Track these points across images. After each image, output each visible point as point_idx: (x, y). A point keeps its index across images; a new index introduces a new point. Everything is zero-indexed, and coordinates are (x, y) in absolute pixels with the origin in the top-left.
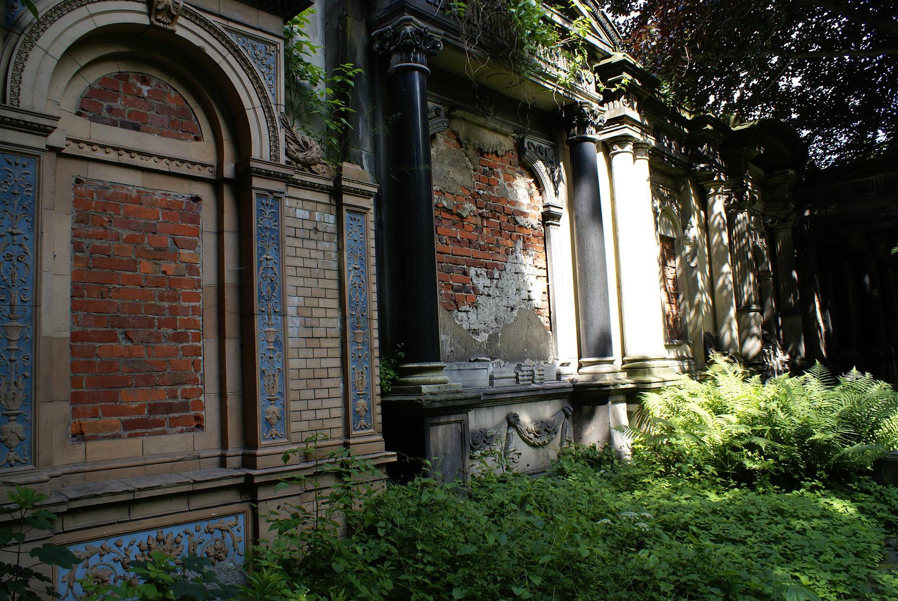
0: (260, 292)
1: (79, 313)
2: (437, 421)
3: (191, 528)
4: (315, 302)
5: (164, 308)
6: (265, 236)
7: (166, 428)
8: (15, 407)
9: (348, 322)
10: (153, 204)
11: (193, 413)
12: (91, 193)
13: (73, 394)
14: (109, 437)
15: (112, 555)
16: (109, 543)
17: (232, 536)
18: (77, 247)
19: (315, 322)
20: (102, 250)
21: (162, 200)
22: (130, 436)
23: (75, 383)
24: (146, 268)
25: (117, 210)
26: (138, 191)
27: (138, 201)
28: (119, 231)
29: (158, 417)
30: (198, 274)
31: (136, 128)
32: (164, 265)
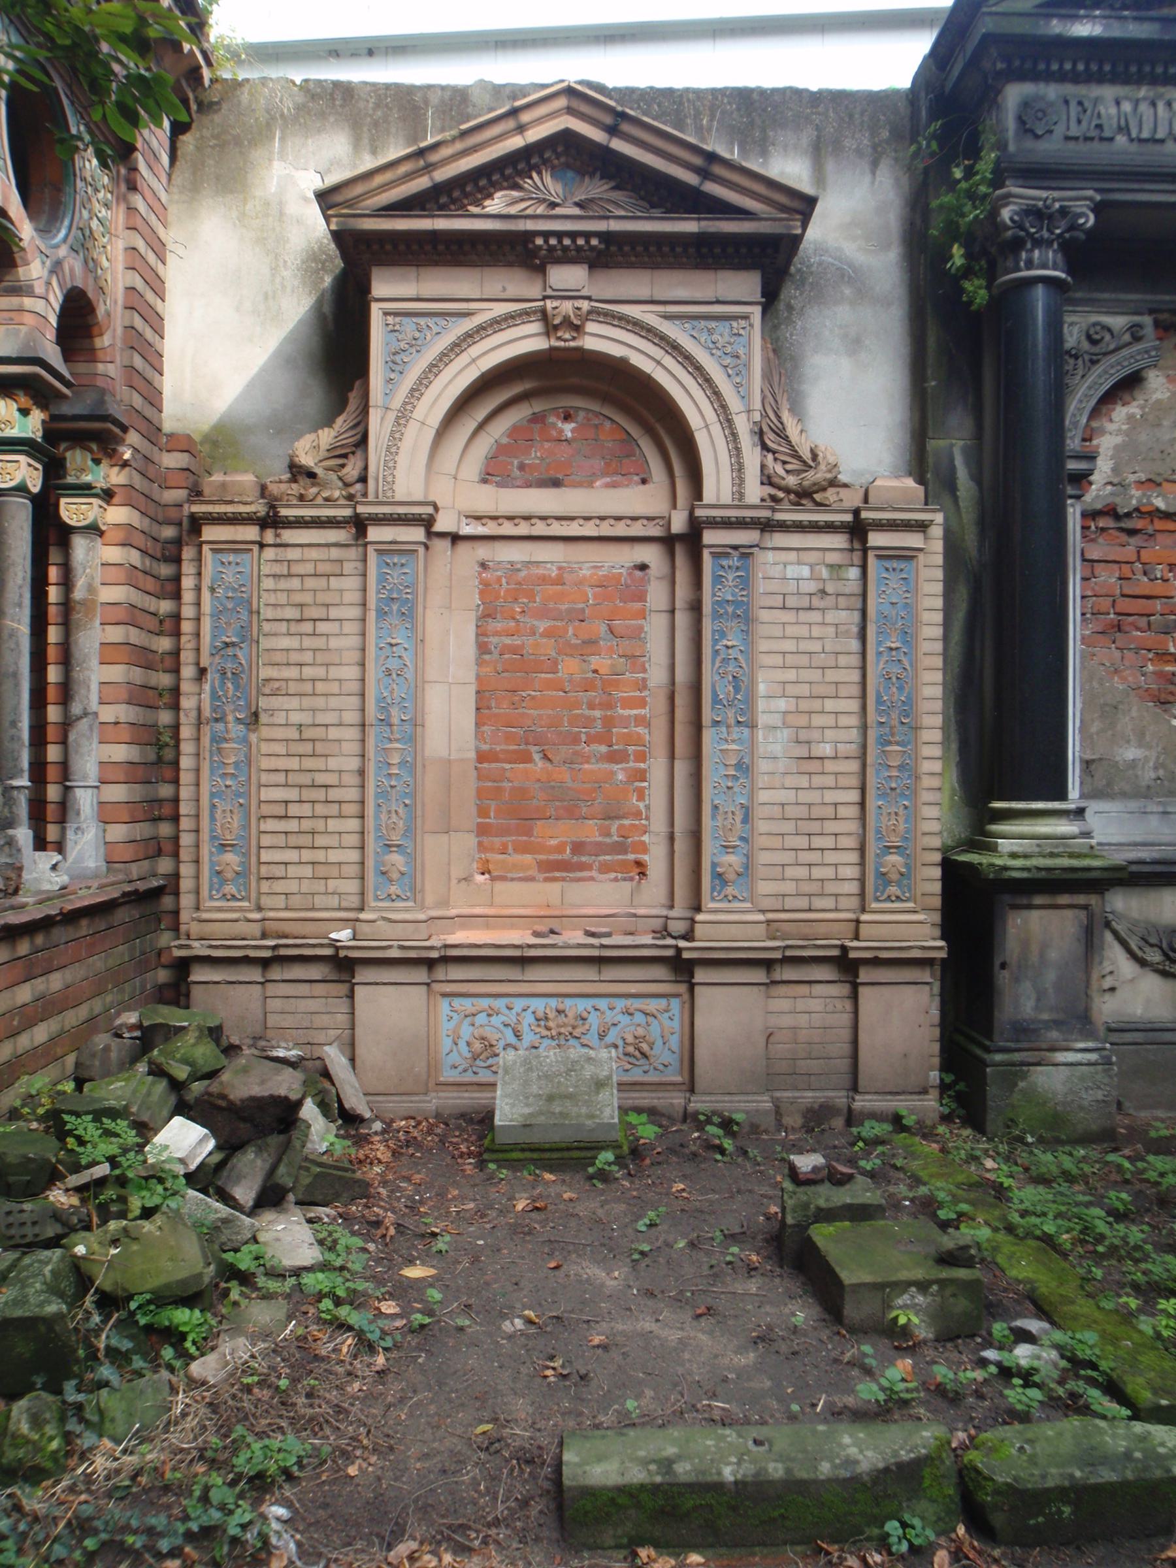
0: (715, 694)
1: (485, 728)
2: (1025, 901)
3: (602, 1004)
4: (816, 705)
5: (595, 720)
6: (726, 613)
7: (594, 874)
8: (396, 839)
9: (872, 734)
10: (581, 582)
11: (631, 857)
12: (499, 579)
13: (479, 824)
14: (521, 879)
15: (502, 1018)
16: (500, 1003)
17: (661, 1024)
18: (482, 648)
19: (815, 735)
20: (514, 650)
21: (592, 576)
22: (546, 880)
23: (482, 812)
24: (569, 667)
25: (531, 596)
26: (560, 568)
27: (559, 581)
28: (536, 623)
29: (583, 859)
30: (645, 671)
31: (556, 483)
32: (595, 661)
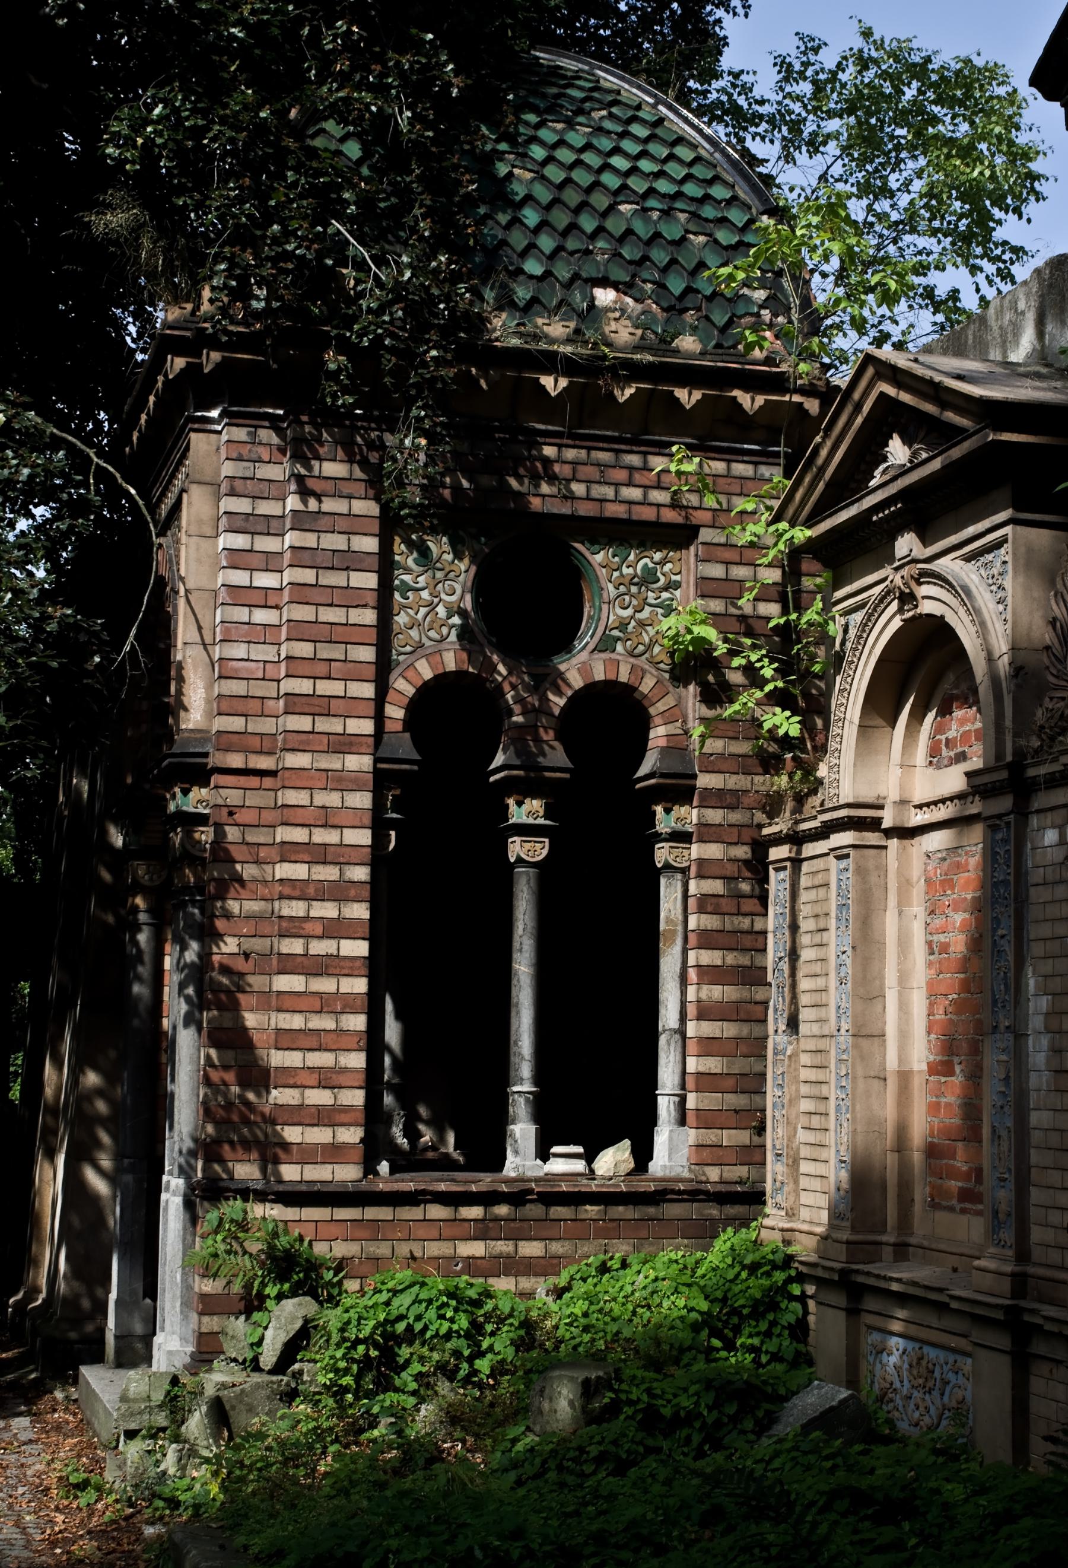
22: (963, 1211)
